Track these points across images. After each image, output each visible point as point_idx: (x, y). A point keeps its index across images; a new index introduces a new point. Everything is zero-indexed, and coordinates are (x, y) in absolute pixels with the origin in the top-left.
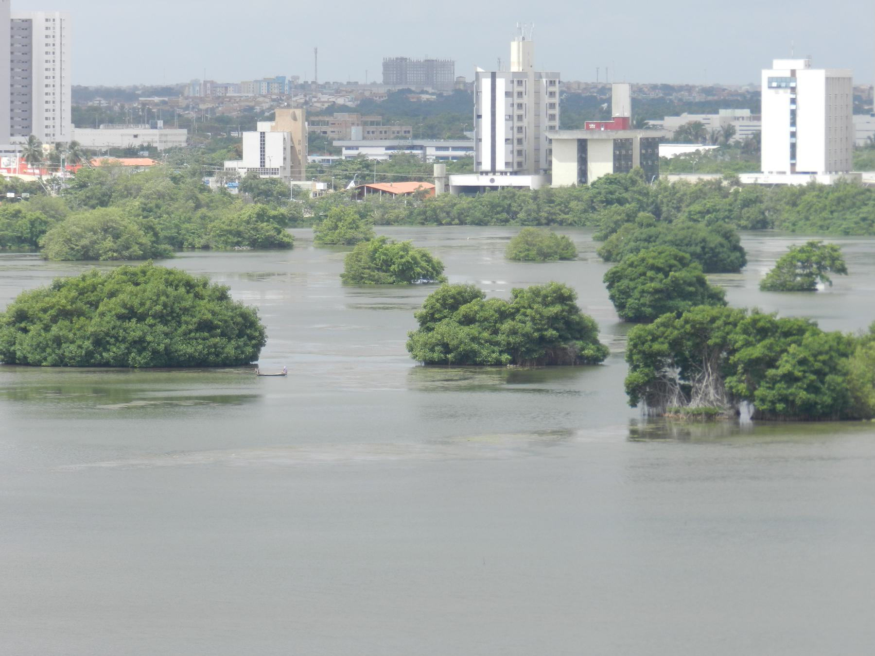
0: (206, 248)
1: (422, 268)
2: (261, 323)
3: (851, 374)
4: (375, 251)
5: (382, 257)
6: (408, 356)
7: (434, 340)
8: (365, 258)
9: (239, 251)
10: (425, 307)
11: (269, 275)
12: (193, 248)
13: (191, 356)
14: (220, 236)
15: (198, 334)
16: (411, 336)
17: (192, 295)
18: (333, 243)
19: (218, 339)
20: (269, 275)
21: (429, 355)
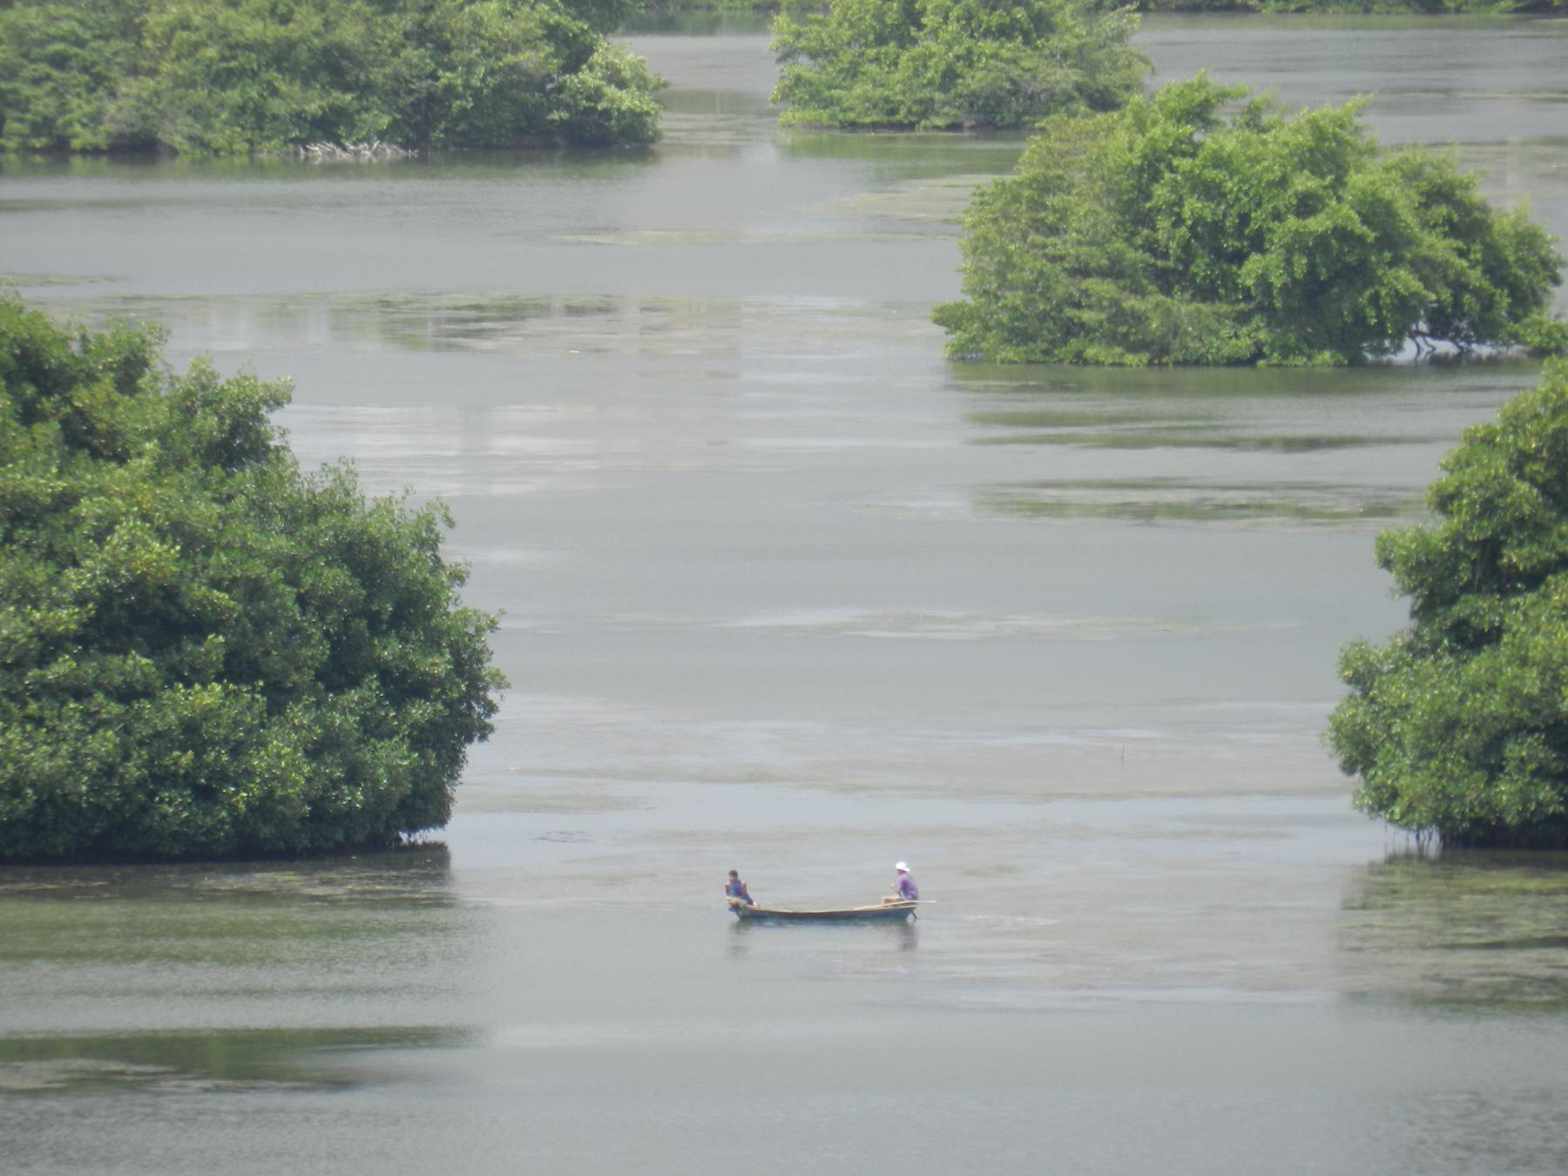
0: (137, 149)
1: (1426, 268)
2: (465, 600)
3: (1419, 245)
4: (1152, 167)
5: (1193, 206)
6: (1343, 793)
7: (1495, 704)
8: (1087, 211)
9: (332, 170)
10: (1445, 502)
11: (514, 312)
12: (57, 151)
13: (52, 798)
14: (222, 79)
15: (90, 668)
16: (1362, 678)
17: (47, 431)
18: (893, 122)
19: (210, 695)
20: (514, 312)
21: (1472, 791)
